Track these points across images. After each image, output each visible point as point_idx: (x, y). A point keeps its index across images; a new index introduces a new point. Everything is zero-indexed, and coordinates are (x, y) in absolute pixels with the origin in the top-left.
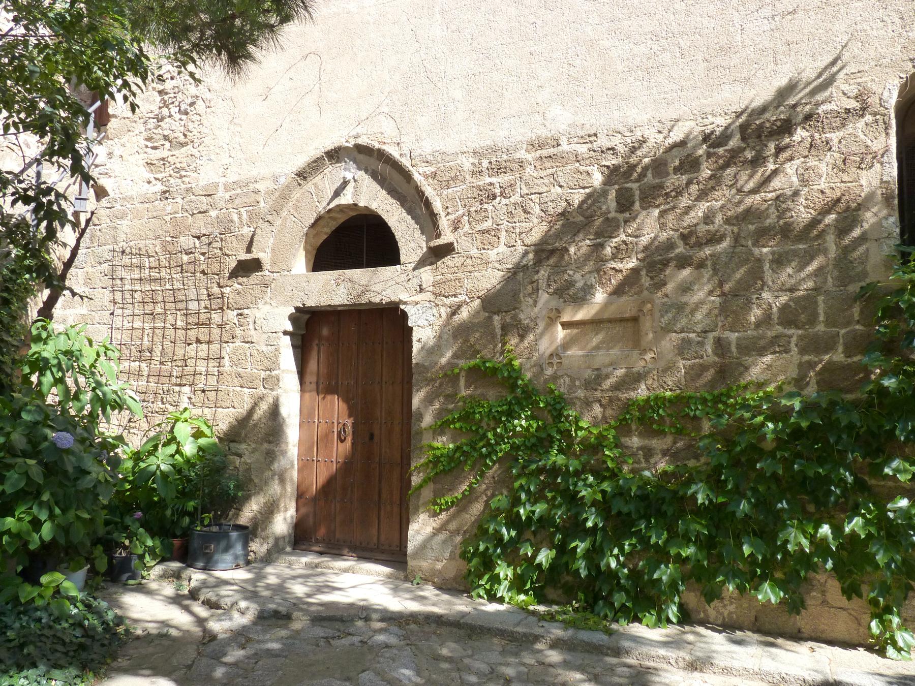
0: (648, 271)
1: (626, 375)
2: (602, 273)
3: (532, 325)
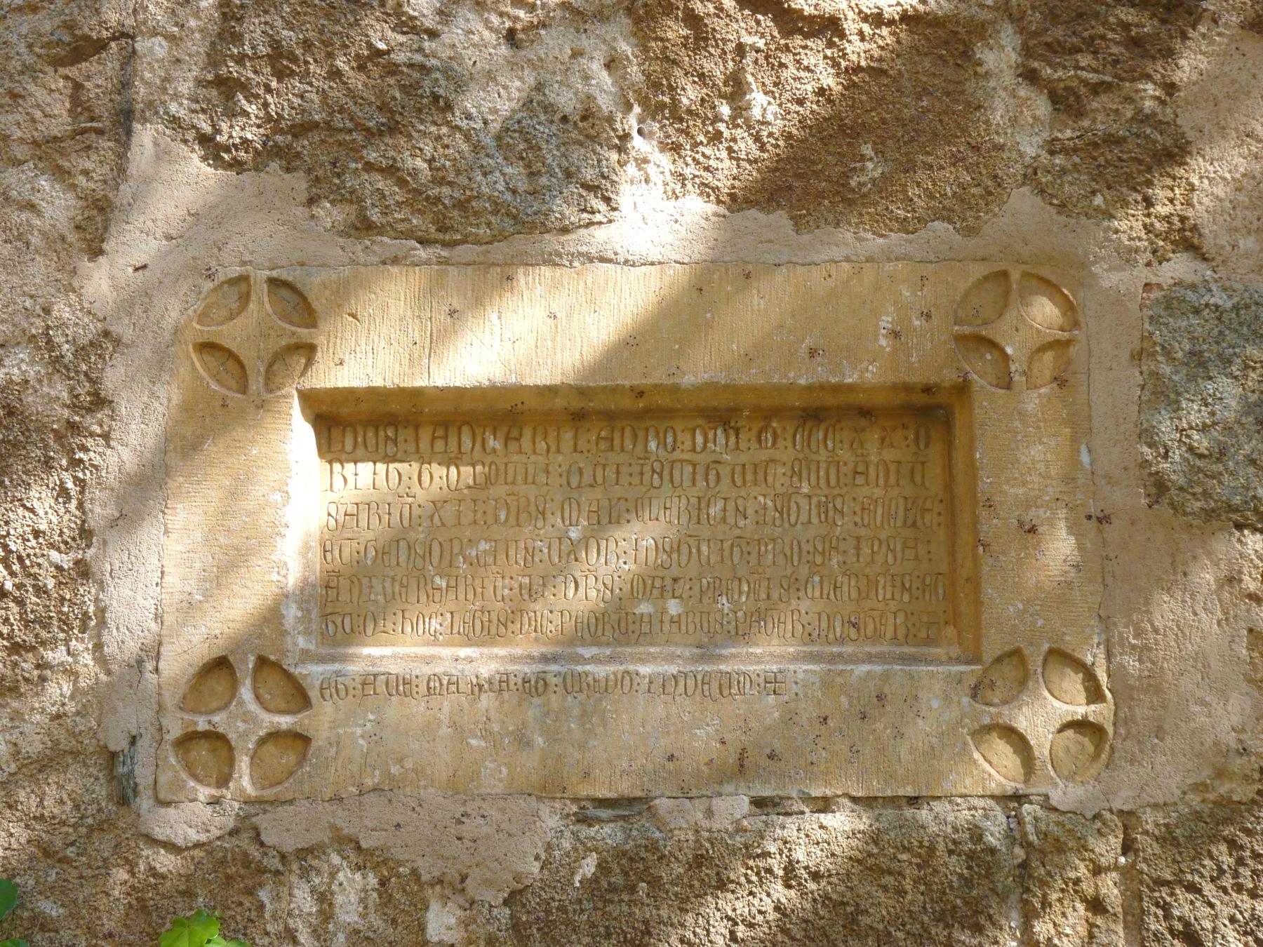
0: (1036, 50)
1: (870, 863)
2: (675, 31)
3: (51, 399)
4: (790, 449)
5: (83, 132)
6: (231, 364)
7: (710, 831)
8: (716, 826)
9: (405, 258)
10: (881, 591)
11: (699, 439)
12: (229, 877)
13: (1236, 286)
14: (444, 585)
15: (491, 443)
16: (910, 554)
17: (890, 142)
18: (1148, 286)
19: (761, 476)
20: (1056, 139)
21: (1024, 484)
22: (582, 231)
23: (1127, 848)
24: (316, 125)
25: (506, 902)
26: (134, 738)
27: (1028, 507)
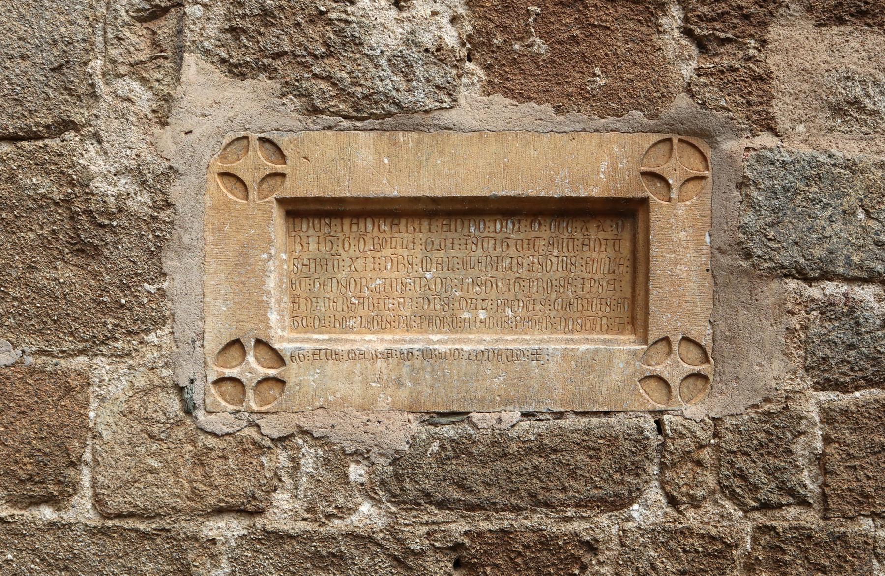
4: (548, 232)
5: (157, 58)
6: (238, 184)
7: (500, 429)
8: (503, 427)
9: (336, 126)
10: (594, 306)
11: (498, 226)
12: (244, 450)
13: (793, 150)
14: (357, 302)
15: (383, 227)
16: (611, 287)
17: (610, 67)
18: (747, 149)
19: (531, 246)
20: (702, 68)
21: (675, 252)
22: (437, 113)
23: (716, 435)
24: (286, 53)
25: (390, 464)
26: (192, 380)
27: (676, 264)
